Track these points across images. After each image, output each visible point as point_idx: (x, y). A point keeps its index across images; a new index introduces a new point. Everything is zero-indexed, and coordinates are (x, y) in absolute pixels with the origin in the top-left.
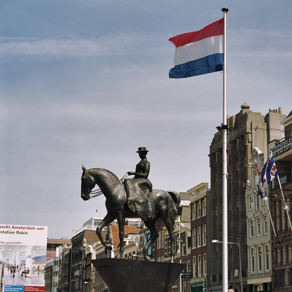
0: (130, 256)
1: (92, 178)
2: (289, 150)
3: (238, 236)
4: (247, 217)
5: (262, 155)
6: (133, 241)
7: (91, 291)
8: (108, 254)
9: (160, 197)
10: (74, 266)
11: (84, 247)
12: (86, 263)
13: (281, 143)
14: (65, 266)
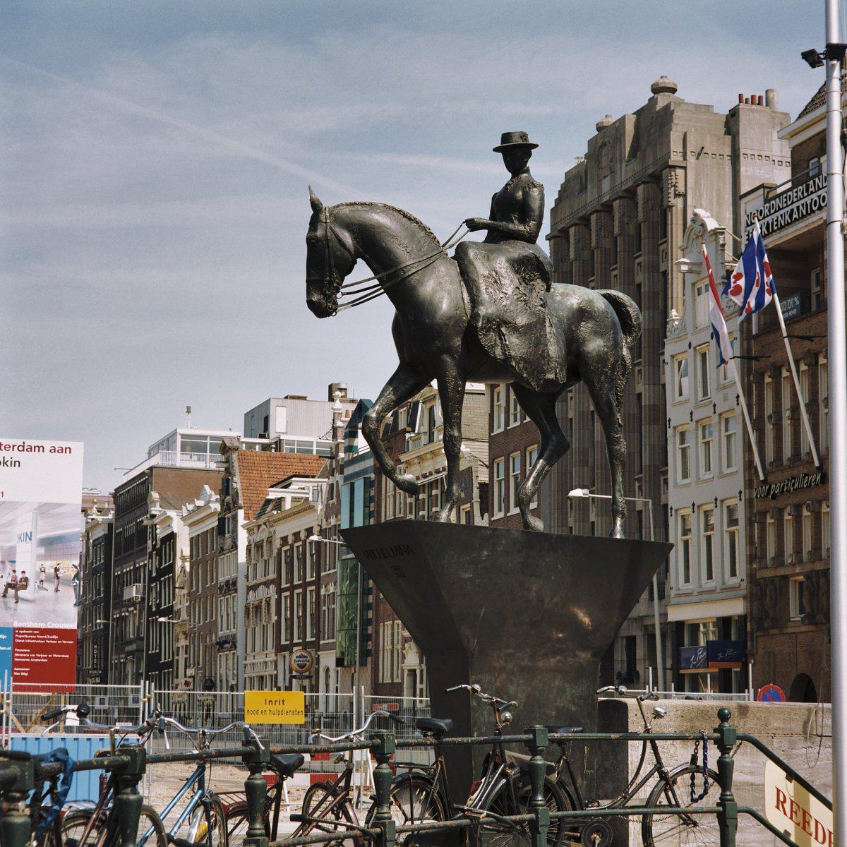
0: (283, 545)
1: (347, 238)
2: (810, 214)
3: (639, 480)
4: (670, 420)
5: (717, 233)
6: (307, 496)
7: (174, 643)
8: (227, 535)
9: (581, 308)
10: (122, 571)
11: (153, 516)
12: (160, 564)
13: (785, 196)
14: (95, 571)
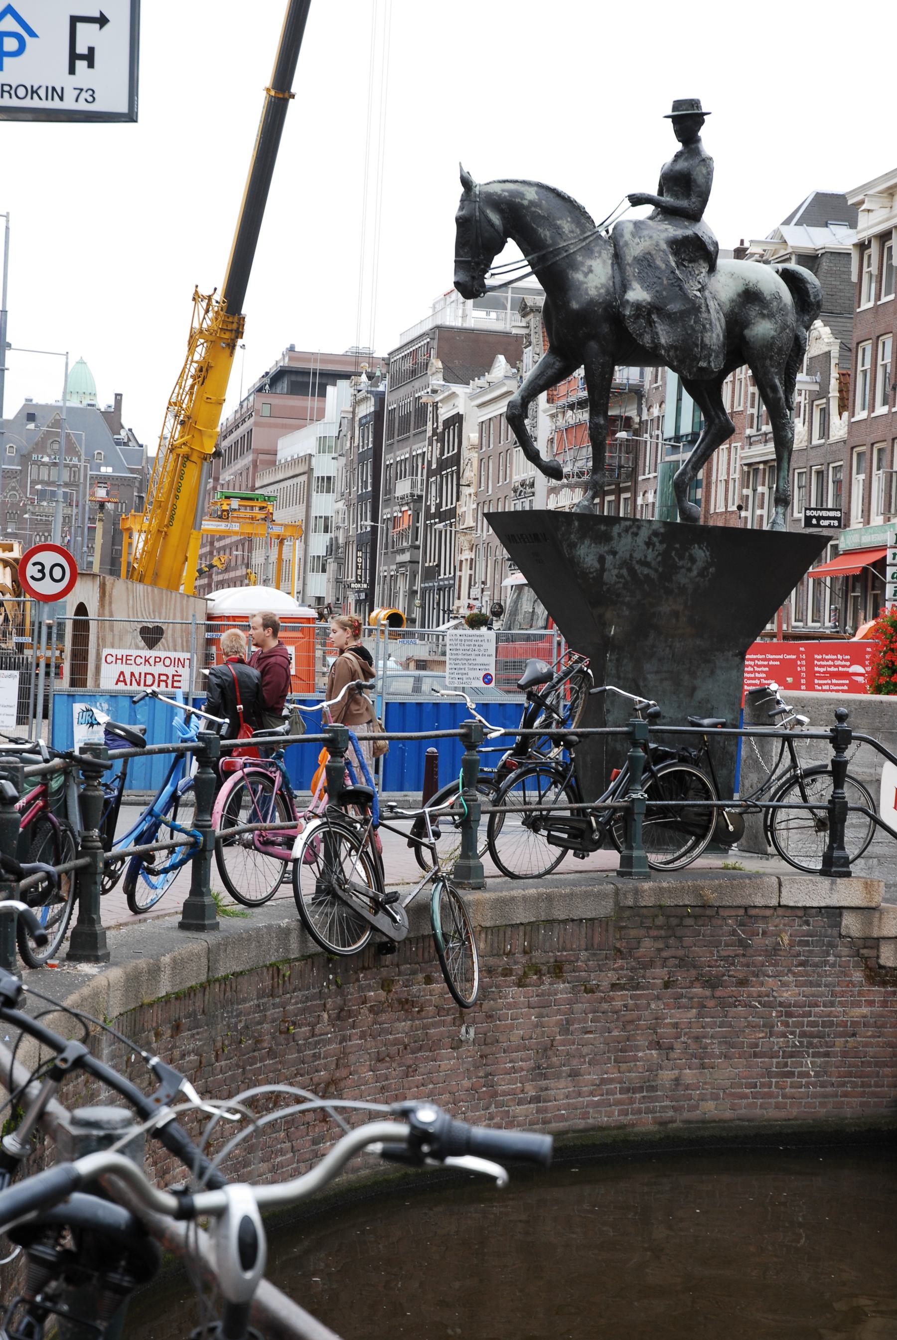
1: (495, 218)
12: (442, 454)
